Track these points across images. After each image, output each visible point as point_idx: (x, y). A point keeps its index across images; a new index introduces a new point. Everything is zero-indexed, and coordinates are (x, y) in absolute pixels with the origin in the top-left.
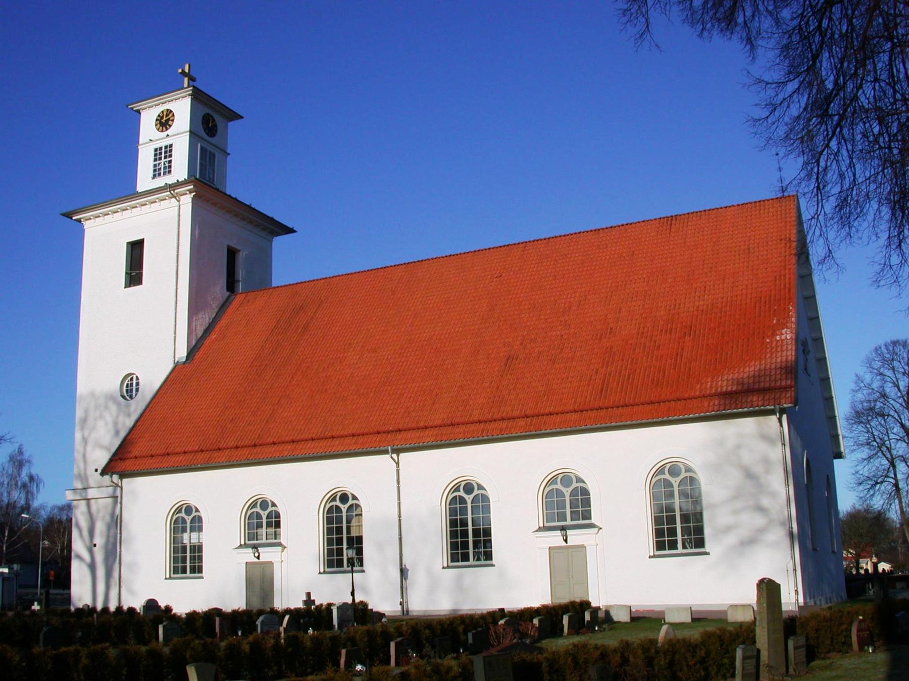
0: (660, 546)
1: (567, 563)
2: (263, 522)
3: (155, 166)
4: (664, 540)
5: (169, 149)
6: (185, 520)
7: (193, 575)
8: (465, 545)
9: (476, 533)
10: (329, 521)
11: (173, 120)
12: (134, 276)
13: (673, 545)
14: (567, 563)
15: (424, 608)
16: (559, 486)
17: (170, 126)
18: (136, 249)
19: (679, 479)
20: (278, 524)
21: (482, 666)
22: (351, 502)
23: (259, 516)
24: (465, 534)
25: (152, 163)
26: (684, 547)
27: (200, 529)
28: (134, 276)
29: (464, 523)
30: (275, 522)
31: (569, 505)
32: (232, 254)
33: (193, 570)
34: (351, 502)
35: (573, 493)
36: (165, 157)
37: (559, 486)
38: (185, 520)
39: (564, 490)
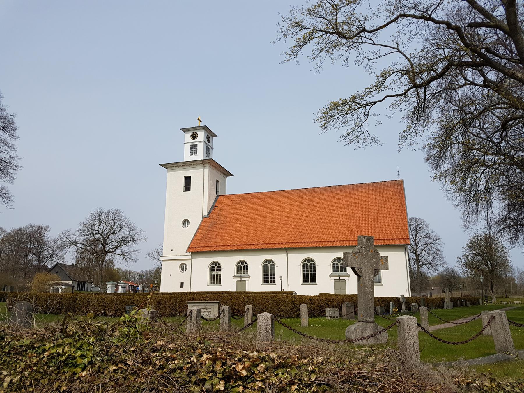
0: (304, 281)
1: (241, 283)
2: (243, 268)
4: (305, 280)
8: (268, 278)
9: (271, 275)
10: (304, 268)
12: (187, 187)
13: (308, 281)
14: (241, 283)
16: (307, 262)
18: (188, 179)
20: (247, 269)
21: (437, 328)
23: (214, 267)
24: (268, 275)
27: (220, 270)
28: (187, 187)
30: (246, 268)
32: (217, 182)
33: (311, 281)
35: (311, 264)
37: (307, 262)
38: (216, 267)
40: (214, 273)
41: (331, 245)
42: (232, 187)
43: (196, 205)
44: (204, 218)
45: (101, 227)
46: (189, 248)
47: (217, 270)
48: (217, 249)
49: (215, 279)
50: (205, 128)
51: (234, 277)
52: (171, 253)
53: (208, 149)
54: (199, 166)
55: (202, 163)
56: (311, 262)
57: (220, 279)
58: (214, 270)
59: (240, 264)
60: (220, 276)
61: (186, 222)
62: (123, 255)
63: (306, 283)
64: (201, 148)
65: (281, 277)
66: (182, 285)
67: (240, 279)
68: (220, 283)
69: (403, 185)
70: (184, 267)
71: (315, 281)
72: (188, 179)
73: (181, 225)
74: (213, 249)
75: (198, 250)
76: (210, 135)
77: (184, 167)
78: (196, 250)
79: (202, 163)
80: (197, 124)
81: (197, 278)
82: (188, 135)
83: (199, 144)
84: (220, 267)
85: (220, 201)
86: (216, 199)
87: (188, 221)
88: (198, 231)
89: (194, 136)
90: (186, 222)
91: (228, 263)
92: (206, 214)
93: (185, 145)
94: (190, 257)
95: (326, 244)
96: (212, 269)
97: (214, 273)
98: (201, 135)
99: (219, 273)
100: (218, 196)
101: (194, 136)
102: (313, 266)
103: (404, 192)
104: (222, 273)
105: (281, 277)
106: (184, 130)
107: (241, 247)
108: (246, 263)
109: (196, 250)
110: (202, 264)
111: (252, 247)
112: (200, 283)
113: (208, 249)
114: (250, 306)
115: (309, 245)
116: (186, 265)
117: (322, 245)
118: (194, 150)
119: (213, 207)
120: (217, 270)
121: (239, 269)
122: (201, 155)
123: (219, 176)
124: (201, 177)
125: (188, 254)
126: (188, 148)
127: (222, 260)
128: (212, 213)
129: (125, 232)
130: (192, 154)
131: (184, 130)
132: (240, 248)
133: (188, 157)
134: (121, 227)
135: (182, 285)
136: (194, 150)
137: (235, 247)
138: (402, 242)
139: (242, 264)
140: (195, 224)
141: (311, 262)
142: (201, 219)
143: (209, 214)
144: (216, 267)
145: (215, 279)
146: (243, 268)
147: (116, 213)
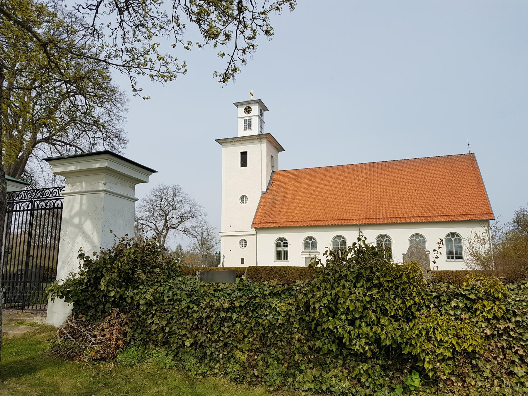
12: (244, 163)
18: (244, 155)
25: (243, 124)
27: (287, 246)
28: (244, 163)
32: (272, 157)
33: (457, 258)
38: (282, 243)
40: (279, 249)
41: (408, 221)
42: (286, 162)
43: (254, 181)
44: (263, 194)
45: (163, 203)
46: (253, 224)
47: (284, 246)
48: (283, 225)
49: (282, 255)
50: (260, 102)
51: (302, 253)
52: (230, 229)
53: (262, 122)
54: (255, 141)
55: (260, 137)
56: (386, 239)
57: (287, 255)
58: (280, 246)
59: (280, 241)
61: (244, 199)
62: (184, 231)
64: (255, 122)
66: (243, 261)
67: (309, 256)
68: (287, 259)
69: (475, 159)
70: (244, 243)
72: (244, 155)
73: (239, 201)
74: (279, 225)
75: (264, 225)
76: (263, 109)
77: (232, 143)
78: (261, 226)
79: (260, 137)
80: (250, 98)
81: (262, 253)
82: (241, 110)
83: (253, 119)
84: (287, 243)
85: (275, 176)
86: (272, 176)
87: (246, 196)
88: (259, 207)
89: (248, 111)
90: (244, 199)
91: (296, 240)
92: (264, 189)
93: (239, 120)
94: (255, 233)
95: (402, 220)
96: (278, 245)
97: (279, 249)
98: (255, 109)
99: (285, 249)
100: (273, 171)
101: (248, 111)
103: (478, 166)
104: (289, 249)
105: (224, 256)
106: (237, 105)
107: (308, 223)
108: (285, 240)
109: (261, 226)
111: (321, 223)
112: (267, 258)
113: (274, 225)
115: (385, 221)
116: (245, 240)
117: (398, 221)
118: (248, 125)
119: (271, 183)
120: (284, 246)
121: (306, 246)
122: (255, 131)
123: (273, 151)
124: (258, 152)
125: (254, 230)
126: (241, 123)
127: (290, 236)
128: (270, 189)
129: (187, 208)
130: (245, 129)
131: (237, 105)
132: (308, 224)
133: (242, 133)
134: (182, 203)
135: (243, 261)
136: (248, 125)
137: (302, 223)
138: (486, 217)
139: (282, 241)
140: (254, 200)
142: (260, 196)
143: (267, 190)
144: (282, 243)
145: (282, 255)
146: (310, 243)
147: (175, 189)
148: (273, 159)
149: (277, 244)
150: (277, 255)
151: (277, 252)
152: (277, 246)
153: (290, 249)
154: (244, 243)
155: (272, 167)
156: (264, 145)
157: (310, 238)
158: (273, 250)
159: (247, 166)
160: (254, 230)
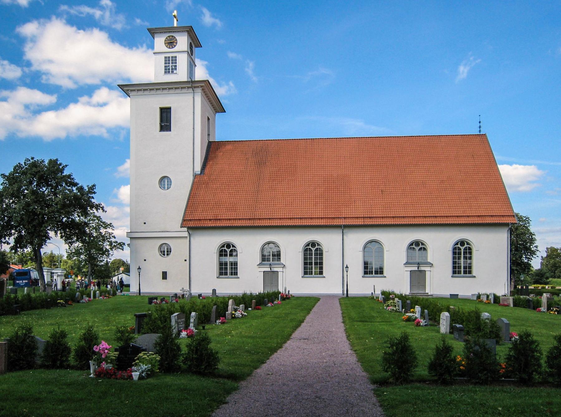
1: (271, 277)
3: (165, 67)
4: (307, 272)
5: (174, 59)
6: (227, 250)
7: (376, 275)
11: (177, 43)
13: (226, 274)
15: (236, 292)
16: (225, 248)
17: (175, 46)
19: (464, 247)
22: (231, 248)
23: (225, 251)
25: (163, 65)
26: (464, 273)
29: (465, 258)
30: (277, 256)
31: (271, 256)
33: (465, 272)
34: (231, 248)
36: (172, 63)
37: (225, 248)
38: (227, 250)
39: (461, 247)
40: (224, 259)
42: (227, 130)
46: (184, 220)
49: (227, 269)
54: (184, 91)
58: (226, 255)
60: (236, 264)
63: (379, 275)
64: (182, 61)
65: (139, 268)
71: (236, 274)
77: (165, 92)
78: (194, 224)
79: (191, 84)
89: (171, 43)
92: (198, 169)
94: (186, 234)
96: (222, 253)
97: (224, 259)
98: (183, 41)
101: (171, 43)
102: (320, 253)
105: (139, 268)
109: (194, 224)
110: (208, 245)
114: (447, 314)
118: (170, 65)
122: (181, 75)
123: (210, 111)
124: (188, 110)
125: (186, 229)
127: (238, 239)
141: (466, 246)
145: (227, 269)
147: (54, 163)
148: (208, 122)
149: (221, 251)
150: (221, 269)
151: (221, 264)
152: (221, 255)
153: (241, 259)
154: (165, 251)
155: (209, 135)
156: (199, 98)
157: (313, 244)
158: (212, 262)
159: (170, 131)
160: (186, 229)
